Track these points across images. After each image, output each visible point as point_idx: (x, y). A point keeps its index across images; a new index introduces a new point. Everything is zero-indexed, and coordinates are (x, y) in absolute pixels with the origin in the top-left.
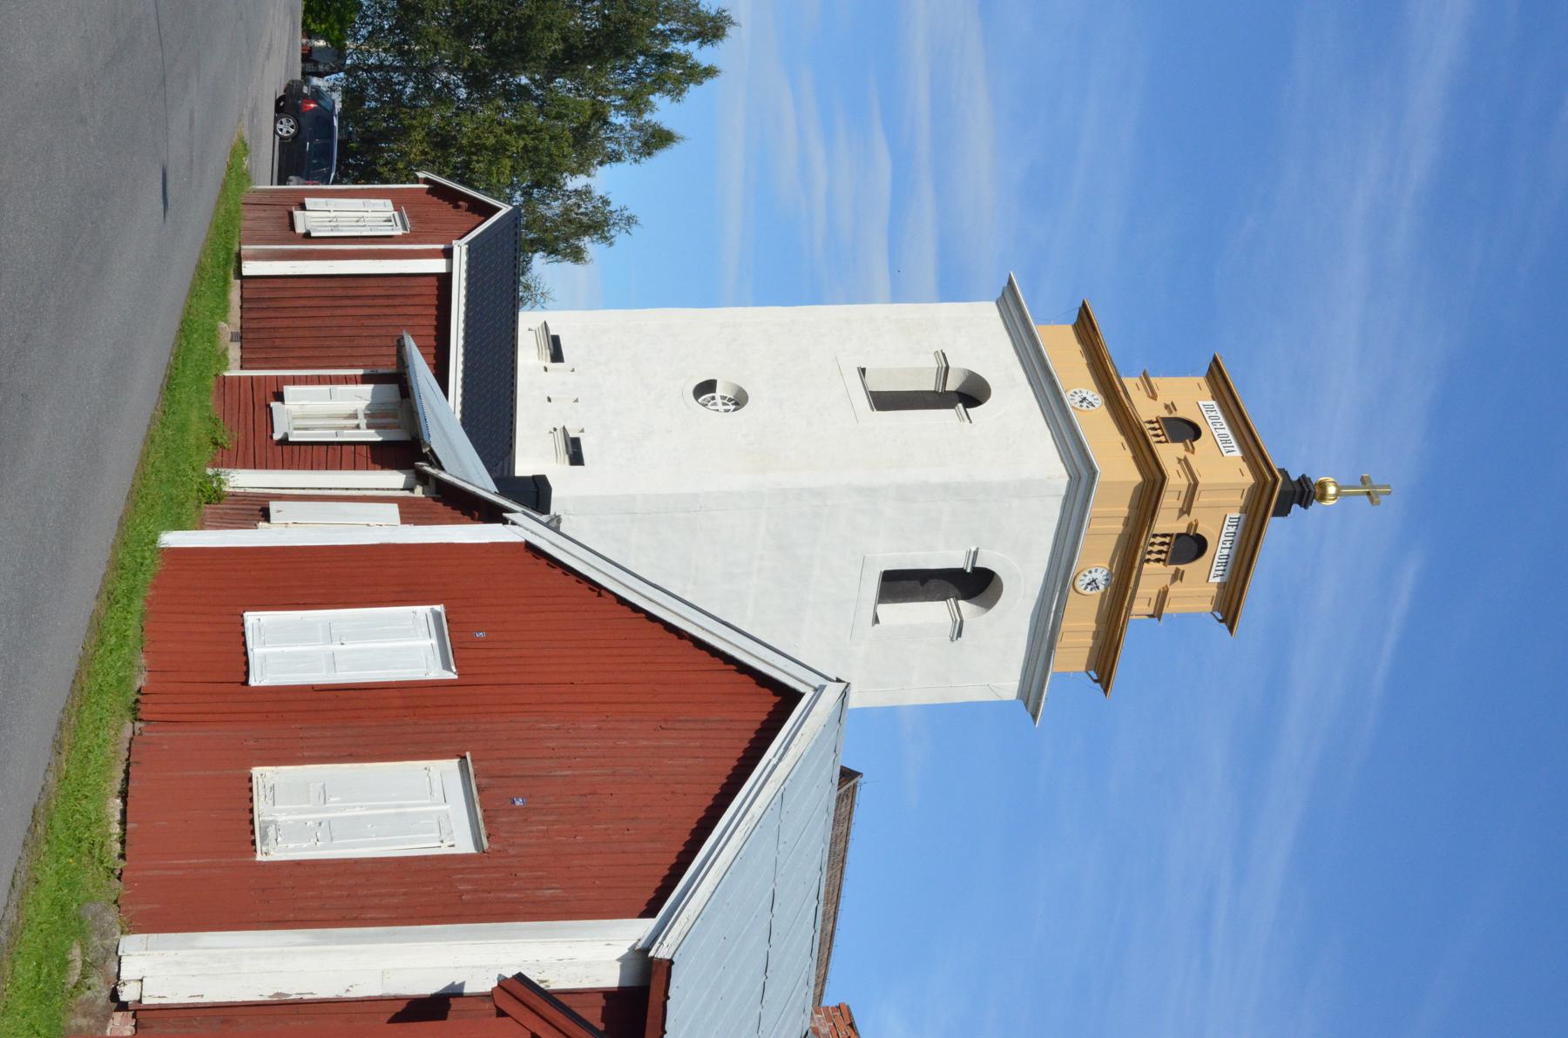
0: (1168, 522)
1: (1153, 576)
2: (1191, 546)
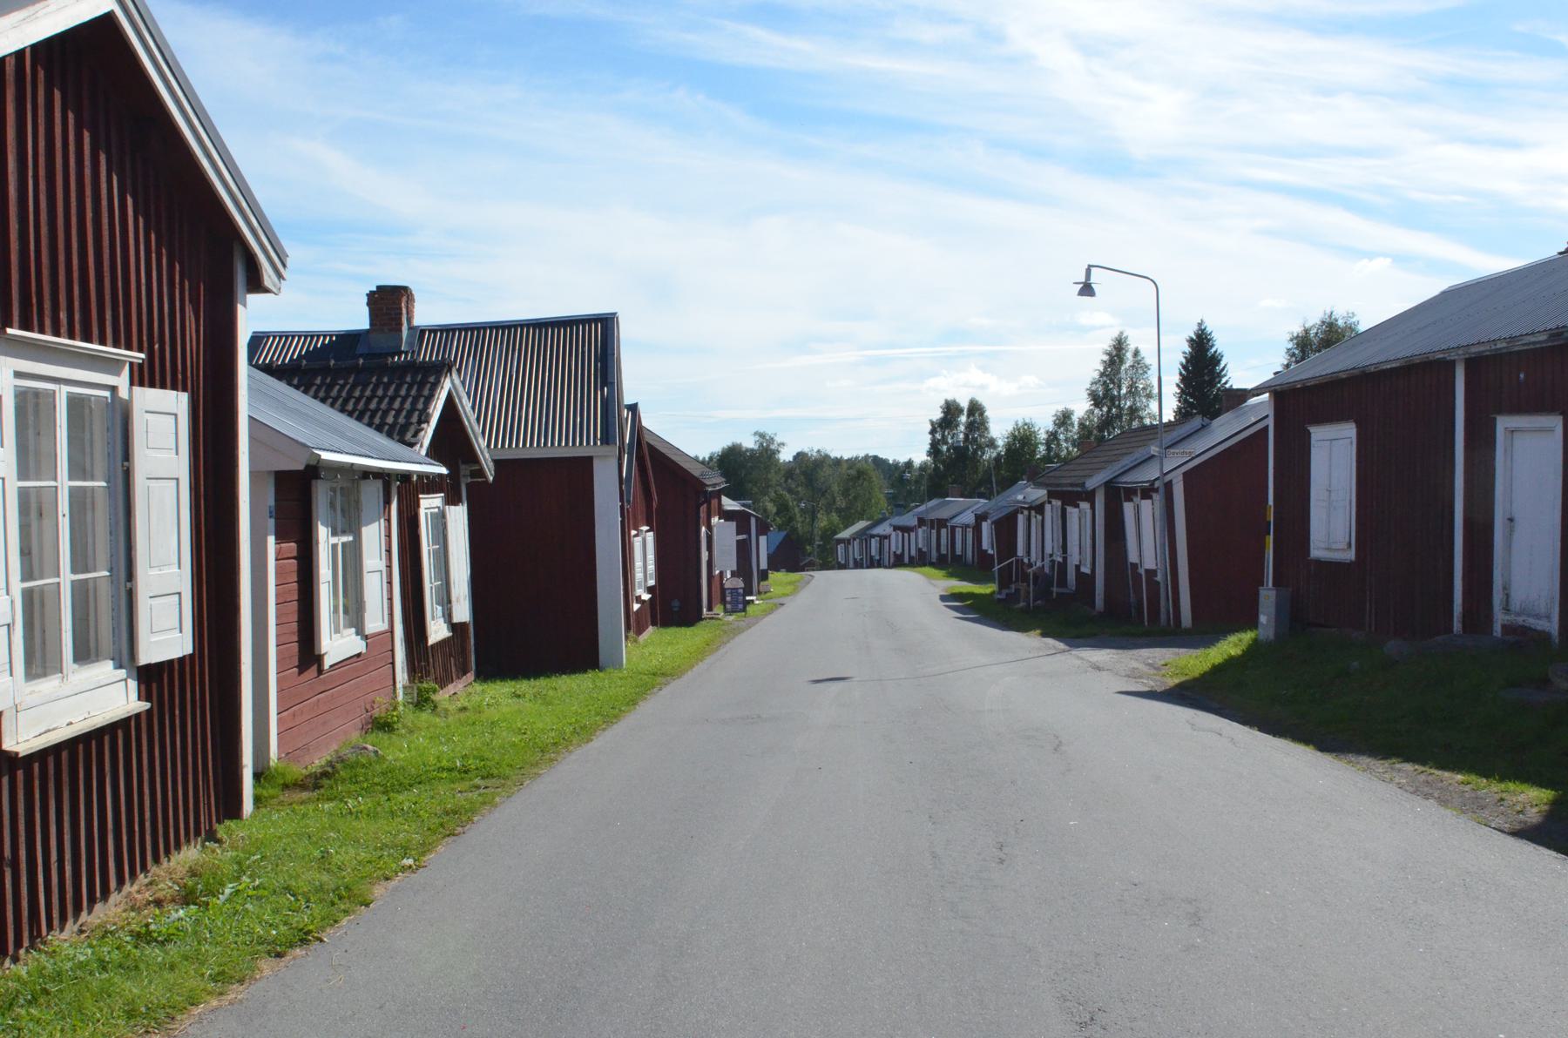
0: (162, 568)
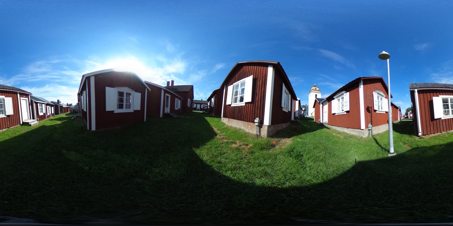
0: (315, 89)
1: (317, 90)
2: (316, 89)
